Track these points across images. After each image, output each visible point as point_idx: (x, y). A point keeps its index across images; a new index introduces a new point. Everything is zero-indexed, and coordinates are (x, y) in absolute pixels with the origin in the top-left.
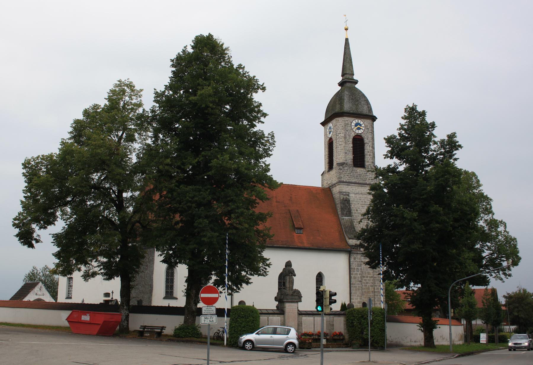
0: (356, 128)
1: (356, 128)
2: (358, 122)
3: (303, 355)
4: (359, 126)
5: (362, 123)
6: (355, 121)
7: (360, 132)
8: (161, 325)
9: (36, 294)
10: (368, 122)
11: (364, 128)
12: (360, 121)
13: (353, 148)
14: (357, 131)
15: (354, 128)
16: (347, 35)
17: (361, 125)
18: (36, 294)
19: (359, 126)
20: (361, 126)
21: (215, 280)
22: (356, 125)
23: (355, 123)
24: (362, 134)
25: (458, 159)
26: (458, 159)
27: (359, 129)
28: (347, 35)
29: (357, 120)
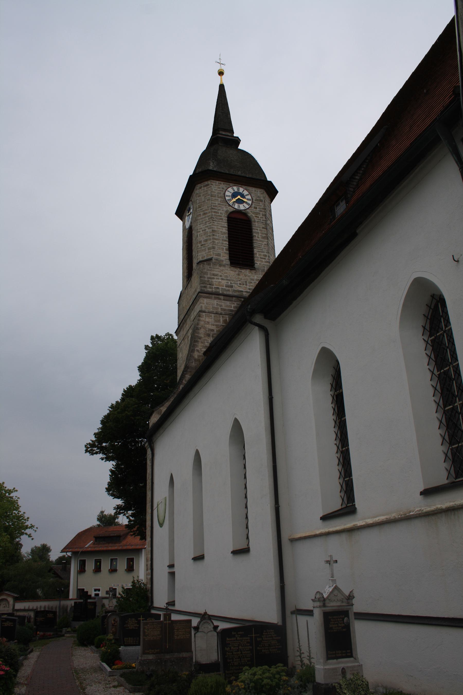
0: (234, 200)
1: (234, 200)
2: (238, 190)
3: (281, 667)
4: (239, 197)
5: (246, 193)
6: (233, 189)
7: (242, 207)
8: (311, 601)
9: (196, 559)
10: (260, 193)
11: (250, 202)
12: (241, 190)
13: (229, 251)
14: (236, 206)
15: (230, 200)
16: (221, 79)
17: (243, 196)
18: (196, 559)
19: (239, 197)
20: (244, 197)
21: (112, 594)
22: (234, 195)
23: (232, 191)
24: (248, 210)
25: (353, 590)
26: (353, 590)
27: (240, 202)
28: (221, 79)
29: (235, 188)
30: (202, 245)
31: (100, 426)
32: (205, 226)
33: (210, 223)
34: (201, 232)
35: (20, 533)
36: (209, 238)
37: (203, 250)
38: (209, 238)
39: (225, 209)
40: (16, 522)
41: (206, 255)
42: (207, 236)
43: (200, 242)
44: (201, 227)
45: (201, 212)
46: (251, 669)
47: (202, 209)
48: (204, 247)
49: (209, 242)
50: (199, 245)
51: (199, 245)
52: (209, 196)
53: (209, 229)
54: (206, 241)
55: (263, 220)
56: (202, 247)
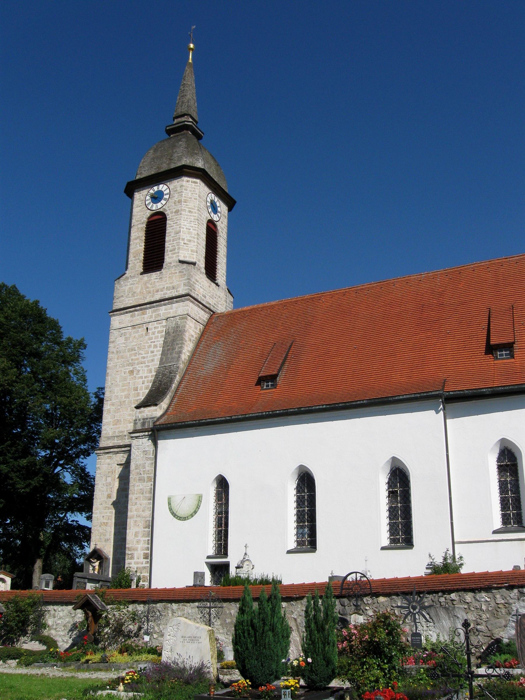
23: (165, 193)
30: (185, 244)
31: (22, 294)
32: (189, 225)
33: (195, 224)
34: (185, 229)
35: (10, 399)
36: (192, 239)
37: (185, 249)
38: (192, 239)
39: (206, 215)
40: (136, 676)
41: (188, 255)
42: (191, 237)
43: (183, 239)
44: (185, 224)
45: (187, 208)
46: (92, 512)
47: (188, 205)
48: (187, 246)
49: (192, 243)
50: (182, 242)
51: (182, 242)
52: (196, 196)
53: (193, 230)
54: (190, 241)
55: (183, 228)
56: (185, 245)
